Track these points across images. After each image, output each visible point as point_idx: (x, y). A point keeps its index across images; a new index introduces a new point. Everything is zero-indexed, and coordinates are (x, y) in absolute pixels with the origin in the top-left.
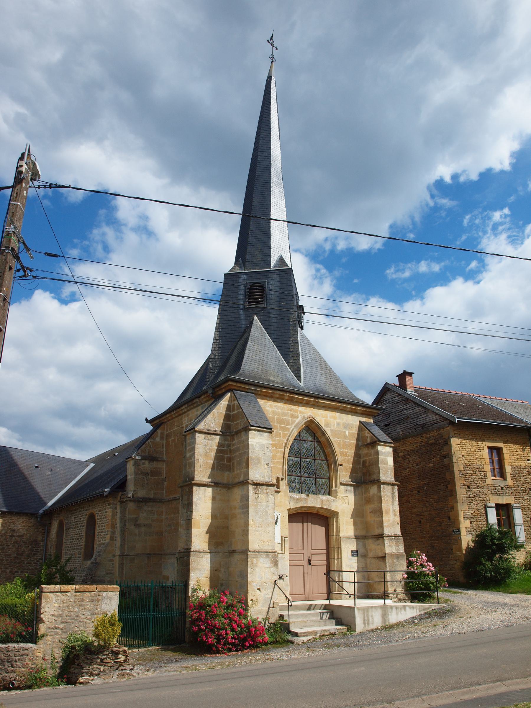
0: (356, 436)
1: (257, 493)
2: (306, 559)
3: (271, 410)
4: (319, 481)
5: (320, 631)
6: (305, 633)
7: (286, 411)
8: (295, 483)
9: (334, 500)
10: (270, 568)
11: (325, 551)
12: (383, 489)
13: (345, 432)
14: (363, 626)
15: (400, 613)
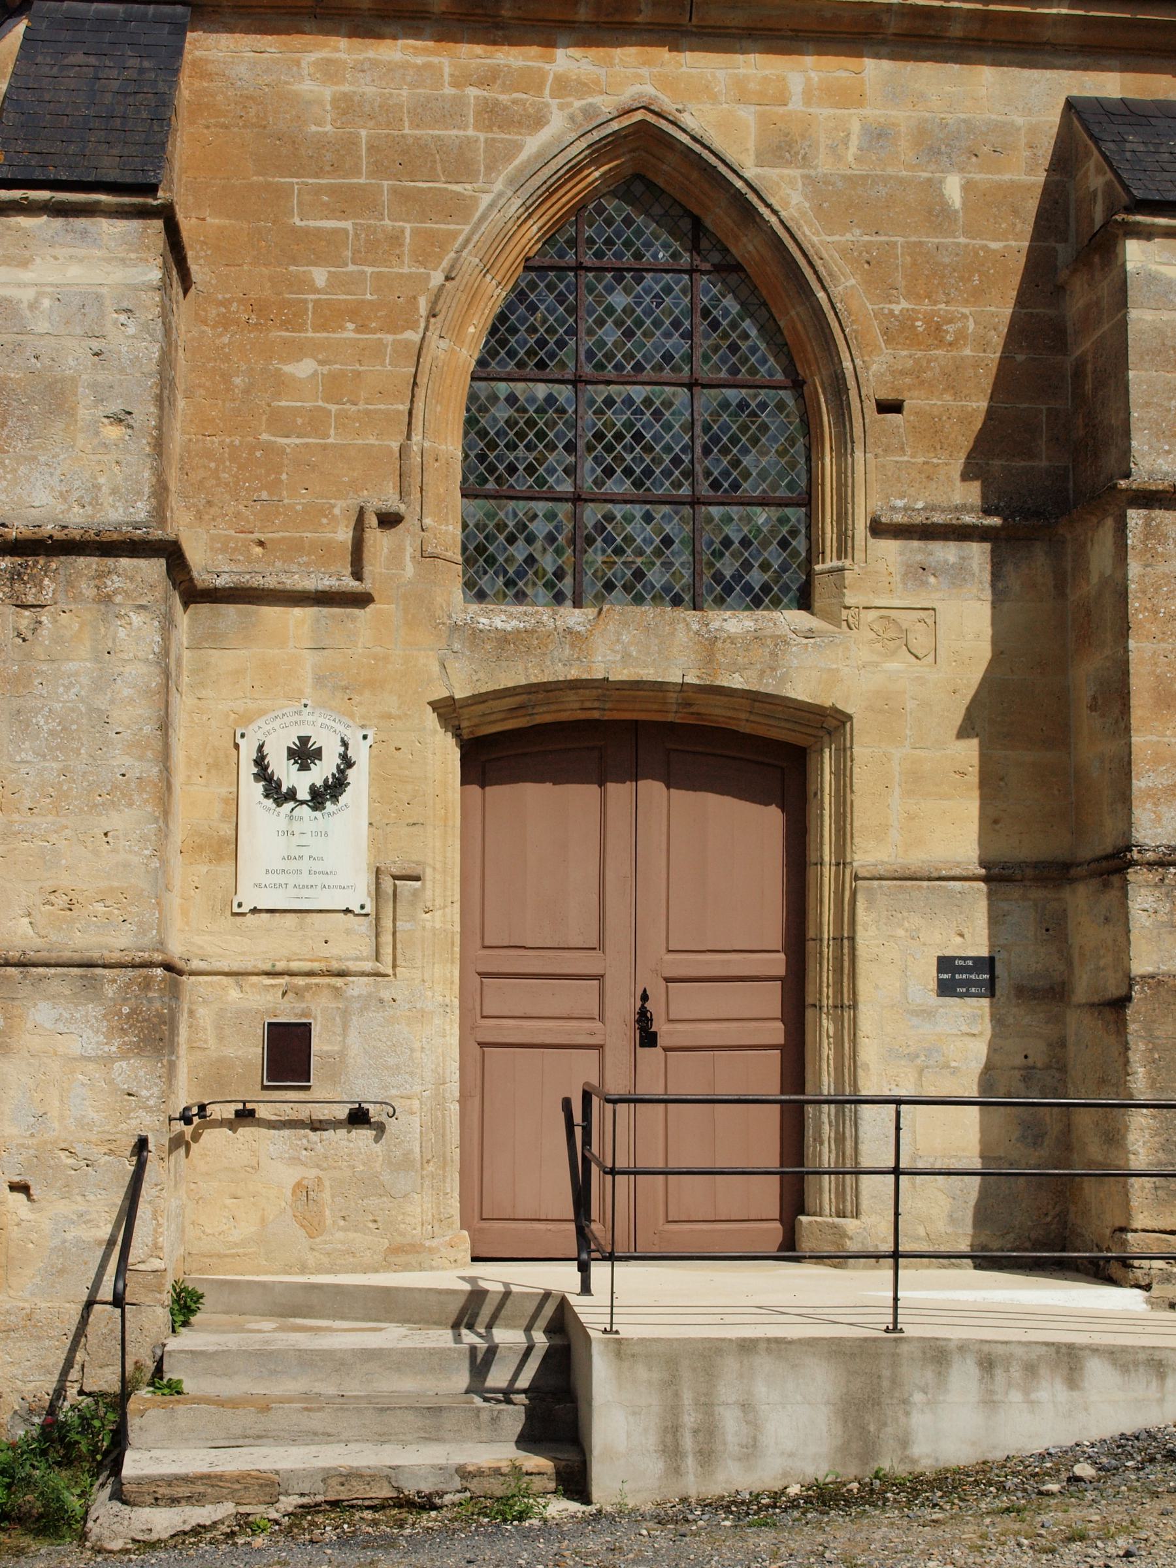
0: (1032, 205)
1: (30, 600)
2: (623, 1008)
3: (327, 93)
4: (728, 519)
5: (309, 1474)
6: (186, 1479)
7: (449, 91)
8: (530, 539)
9: (810, 634)
10: (107, 1061)
11: (777, 964)
12: (1147, 536)
13: (933, 187)
14: (655, 1466)
15: (1016, 1396)
